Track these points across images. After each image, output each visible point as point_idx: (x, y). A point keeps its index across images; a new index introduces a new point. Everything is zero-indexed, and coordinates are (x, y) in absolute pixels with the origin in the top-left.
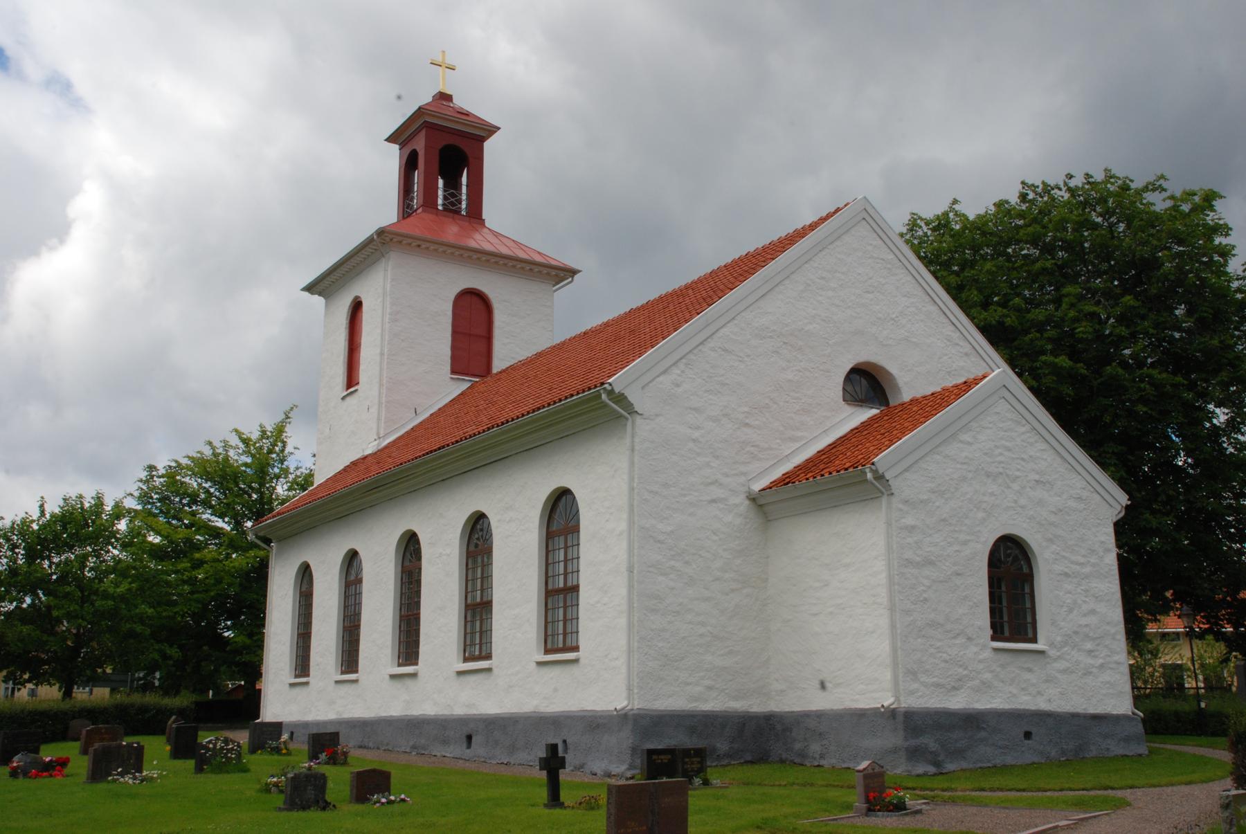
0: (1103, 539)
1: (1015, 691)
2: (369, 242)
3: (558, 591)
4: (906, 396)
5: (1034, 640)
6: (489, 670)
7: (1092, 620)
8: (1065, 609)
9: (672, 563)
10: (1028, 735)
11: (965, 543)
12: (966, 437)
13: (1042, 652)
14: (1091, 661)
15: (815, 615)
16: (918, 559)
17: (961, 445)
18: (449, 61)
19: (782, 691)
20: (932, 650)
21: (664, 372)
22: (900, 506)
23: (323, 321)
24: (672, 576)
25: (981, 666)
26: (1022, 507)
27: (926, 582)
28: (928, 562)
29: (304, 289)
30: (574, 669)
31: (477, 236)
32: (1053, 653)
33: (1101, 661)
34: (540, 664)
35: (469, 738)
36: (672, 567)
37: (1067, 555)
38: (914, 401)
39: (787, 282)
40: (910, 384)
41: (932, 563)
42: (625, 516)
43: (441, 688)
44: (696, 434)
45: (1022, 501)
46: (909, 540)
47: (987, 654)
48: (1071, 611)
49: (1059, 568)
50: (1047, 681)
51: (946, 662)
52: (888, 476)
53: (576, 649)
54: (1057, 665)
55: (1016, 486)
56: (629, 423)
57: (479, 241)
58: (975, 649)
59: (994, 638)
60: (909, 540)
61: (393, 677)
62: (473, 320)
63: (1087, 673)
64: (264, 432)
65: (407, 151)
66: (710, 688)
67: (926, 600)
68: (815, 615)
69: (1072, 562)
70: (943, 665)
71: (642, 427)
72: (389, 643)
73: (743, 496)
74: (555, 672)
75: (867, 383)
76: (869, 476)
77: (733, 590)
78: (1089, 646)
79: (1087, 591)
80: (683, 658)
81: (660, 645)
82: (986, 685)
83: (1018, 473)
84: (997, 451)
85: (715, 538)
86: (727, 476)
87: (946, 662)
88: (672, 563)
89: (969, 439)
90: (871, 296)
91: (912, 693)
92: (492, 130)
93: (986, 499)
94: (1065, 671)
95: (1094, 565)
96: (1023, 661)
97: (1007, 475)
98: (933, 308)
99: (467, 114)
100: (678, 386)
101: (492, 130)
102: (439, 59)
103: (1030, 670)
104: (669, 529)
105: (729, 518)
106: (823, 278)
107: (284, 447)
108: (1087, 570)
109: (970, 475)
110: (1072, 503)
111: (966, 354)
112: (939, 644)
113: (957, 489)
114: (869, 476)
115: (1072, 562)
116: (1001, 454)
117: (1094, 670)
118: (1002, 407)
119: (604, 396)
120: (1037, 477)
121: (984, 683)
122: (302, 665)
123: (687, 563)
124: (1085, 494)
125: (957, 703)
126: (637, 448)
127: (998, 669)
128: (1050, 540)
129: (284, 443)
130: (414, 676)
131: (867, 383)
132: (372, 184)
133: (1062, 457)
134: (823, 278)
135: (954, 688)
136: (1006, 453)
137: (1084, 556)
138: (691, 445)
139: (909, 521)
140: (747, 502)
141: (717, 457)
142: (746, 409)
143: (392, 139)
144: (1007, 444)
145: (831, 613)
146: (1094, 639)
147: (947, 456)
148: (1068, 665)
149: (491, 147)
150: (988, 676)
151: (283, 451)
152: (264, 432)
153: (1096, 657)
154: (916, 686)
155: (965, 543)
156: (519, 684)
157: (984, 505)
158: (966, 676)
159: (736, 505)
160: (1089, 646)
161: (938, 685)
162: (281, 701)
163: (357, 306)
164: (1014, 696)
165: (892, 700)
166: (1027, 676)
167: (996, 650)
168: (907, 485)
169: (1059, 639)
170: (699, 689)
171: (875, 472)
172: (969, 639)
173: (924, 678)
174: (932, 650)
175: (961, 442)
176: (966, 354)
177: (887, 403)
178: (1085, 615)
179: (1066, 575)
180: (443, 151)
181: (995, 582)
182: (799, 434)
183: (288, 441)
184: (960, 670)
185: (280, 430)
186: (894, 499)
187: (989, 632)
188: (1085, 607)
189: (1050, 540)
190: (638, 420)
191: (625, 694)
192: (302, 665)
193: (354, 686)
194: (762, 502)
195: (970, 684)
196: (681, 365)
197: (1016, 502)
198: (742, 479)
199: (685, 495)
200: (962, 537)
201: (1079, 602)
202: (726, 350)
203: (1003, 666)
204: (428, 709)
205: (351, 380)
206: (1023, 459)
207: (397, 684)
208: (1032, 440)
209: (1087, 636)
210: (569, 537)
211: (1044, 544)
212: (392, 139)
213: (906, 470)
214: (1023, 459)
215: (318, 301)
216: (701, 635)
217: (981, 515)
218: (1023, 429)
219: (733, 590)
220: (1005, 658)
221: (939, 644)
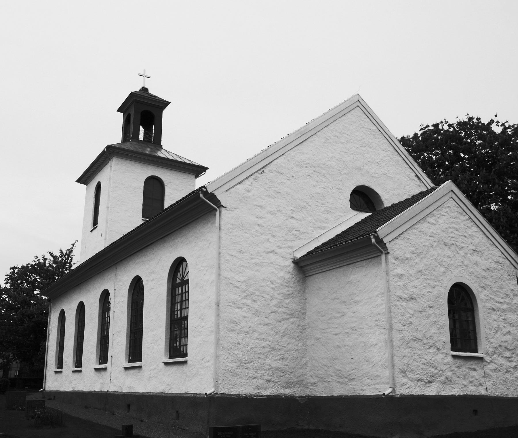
0: (512, 288)
1: (466, 383)
2: (103, 153)
3: (178, 319)
4: (387, 204)
5: (476, 351)
6: (140, 367)
7: (509, 338)
8: (493, 331)
9: (245, 301)
10: (475, 412)
11: (434, 287)
12: (431, 220)
13: (481, 359)
14: (509, 364)
15: (336, 334)
16: (406, 296)
17: (429, 225)
18: (148, 75)
19: (315, 383)
20: (415, 357)
21: (240, 183)
22: (394, 261)
23: (84, 193)
24: (245, 309)
25: (446, 367)
26: (466, 266)
27: (411, 312)
28: (413, 299)
29: (77, 181)
30: (184, 368)
31: (159, 152)
32: (487, 359)
33: (515, 364)
34: (166, 364)
35: (129, 406)
36: (245, 304)
37: (493, 297)
38: (393, 205)
39: (315, 136)
40: (389, 198)
41: (414, 299)
42: (215, 270)
43: (118, 379)
44: (260, 221)
45: (466, 262)
46: (400, 283)
47: (449, 359)
48: (497, 332)
49: (489, 305)
50: (484, 377)
51: (424, 364)
52: (385, 240)
53: (186, 355)
54: (492, 366)
55: (461, 253)
56: (218, 213)
57: (160, 154)
58: (442, 356)
59: (452, 350)
60: (400, 283)
61: (96, 370)
62: (154, 189)
63: (507, 372)
64: (62, 252)
65: (126, 114)
66: (269, 381)
67: (411, 323)
68: (336, 334)
69: (497, 302)
70: (422, 366)
71: (225, 217)
72: (95, 351)
73: (291, 261)
74: (174, 369)
75: (363, 197)
76: (373, 240)
77: (284, 319)
78: (508, 354)
79: (505, 320)
80: (251, 362)
81: (236, 352)
82: (449, 379)
83: (463, 245)
84: (450, 230)
85: (272, 286)
86: (280, 248)
87: (424, 364)
88: (245, 301)
89: (434, 222)
90: (365, 149)
91: (403, 385)
92: (166, 104)
93: (445, 259)
94: (494, 370)
95: (508, 304)
96: (471, 364)
97: (457, 245)
98: (400, 158)
99: (155, 96)
100: (249, 191)
101: (166, 104)
102: (142, 74)
103: (474, 370)
104: (243, 279)
105: (281, 274)
106: (336, 136)
107: (71, 260)
108: (505, 306)
109: (435, 244)
110: (494, 265)
111: (419, 186)
112: (420, 352)
113: (427, 252)
114: (373, 240)
115: (497, 302)
116: (452, 232)
117: (511, 370)
118: (451, 203)
119: (201, 195)
120: (474, 248)
121: (447, 378)
122: (60, 364)
123: (254, 301)
124: (501, 260)
125: (431, 391)
126: (222, 228)
127: (456, 369)
128: (483, 288)
129: (72, 258)
130: (80, 371)
131: (363, 197)
132: (111, 130)
133: (487, 237)
134: (336, 136)
135: (430, 382)
136: (456, 232)
137: (502, 298)
138: (257, 228)
139: (400, 271)
140: (292, 265)
141: (274, 236)
142: (292, 208)
143: (119, 110)
144: (455, 226)
145: (347, 333)
146: (510, 350)
147: (420, 231)
148: (496, 366)
149: (166, 113)
150: (449, 374)
151: (71, 262)
152: (62, 252)
153: (511, 361)
154: (405, 380)
155: (434, 287)
156: (155, 377)
157: (444, 264)
158: (437, 373)
159: (286, 266)
160: (508, 354)
161: (419, 380)
162: (53, 382)
163: (99, 186)
164: (466, 386)
165: (390, 390)
166: (473, 373)
167: (454, 357)
168: (397, 248)
169: (491, 350)
170: (261, 381)
171: (377, 238)
172: (438, 349)
173: (410, 375)
174: (415, 357)
175: (429, 223)
176: (419, 186)
177: (375, 210)
178: (505, 335)
179: (493, 309)
180: (143, 112)
181: (452, 311)
182: (324, 225)
183: (74, 257)
184: (433, 370)
185: (70, 251)
186: (390, 256)
187: (449, 345)
188: (505, 330)
189: (483, 288)
190: (223, 210)
191: (212, 384)
192: (60, 364)
193: (80, 374)
194: (302, 264)
195: (439, 379)
196: (251, 179)
197: (462, 262)
198: (290, 251)
199: (253, 259)
200: (432, 283)
201: (501, 326)
202: (279, 173)
203: (459, 367)
204: (112, 388)
205: (95, 222)
206: (465, 236)
207: (98, 374)
208: (470, 225)
209: (506, 348)
210: (184, 287)
211: (480, 289)
212: (119, 110)
213: (396, 238)
214: (465, 236)
215: (83, 186)
216: (263, 347)
217: (442, 269)
218: (464, 218)
219: (284, 319)
220: (459, 362)
221: (420, 352)
